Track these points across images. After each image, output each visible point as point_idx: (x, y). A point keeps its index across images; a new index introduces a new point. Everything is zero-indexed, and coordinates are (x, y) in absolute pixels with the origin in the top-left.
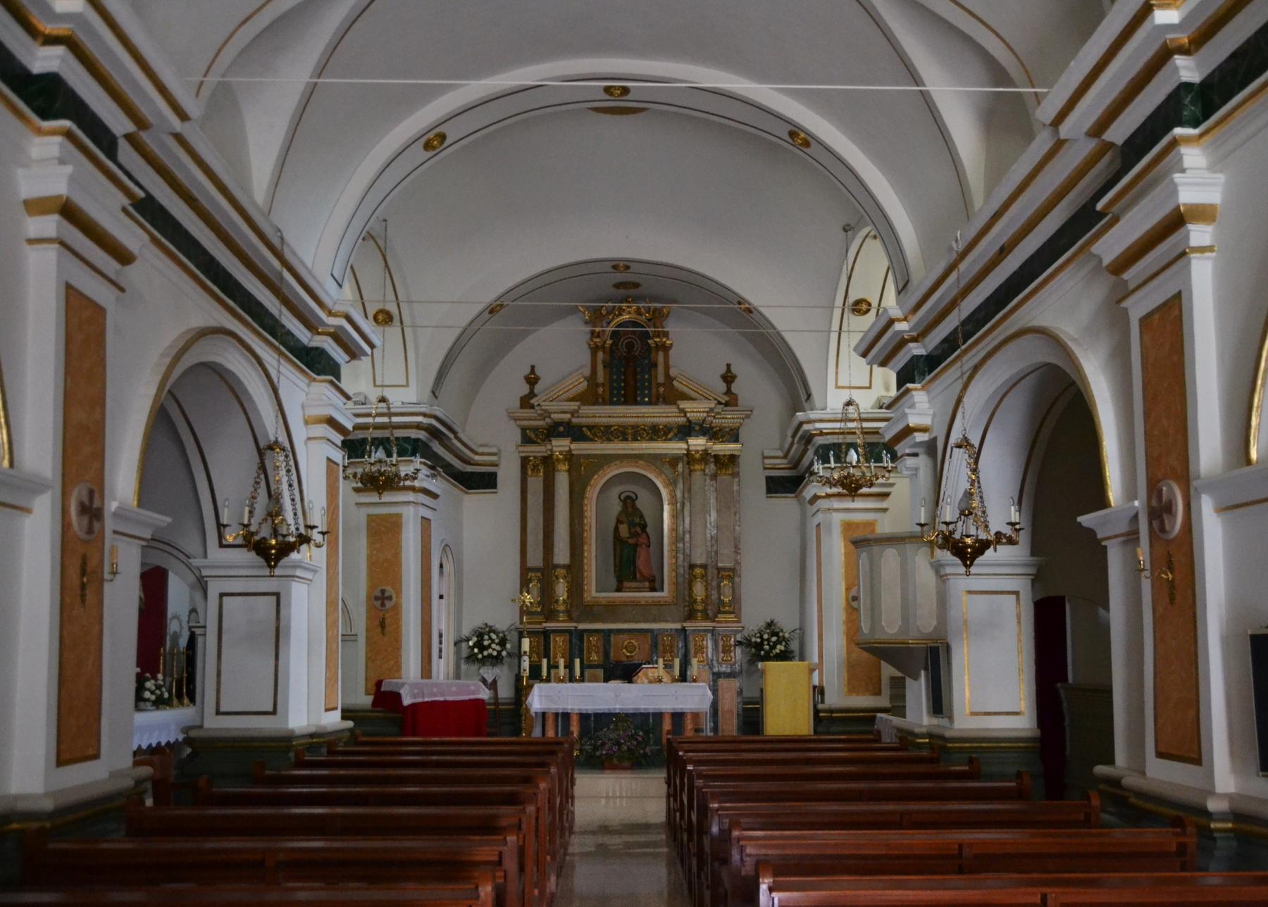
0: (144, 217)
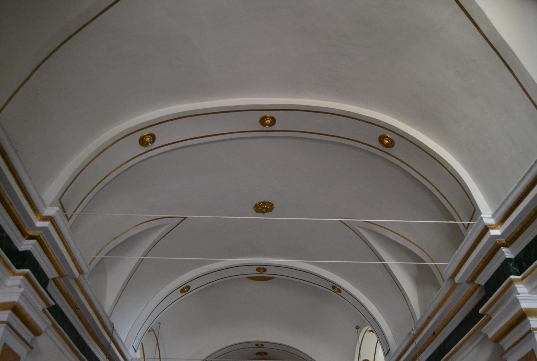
0: (52, 315)
